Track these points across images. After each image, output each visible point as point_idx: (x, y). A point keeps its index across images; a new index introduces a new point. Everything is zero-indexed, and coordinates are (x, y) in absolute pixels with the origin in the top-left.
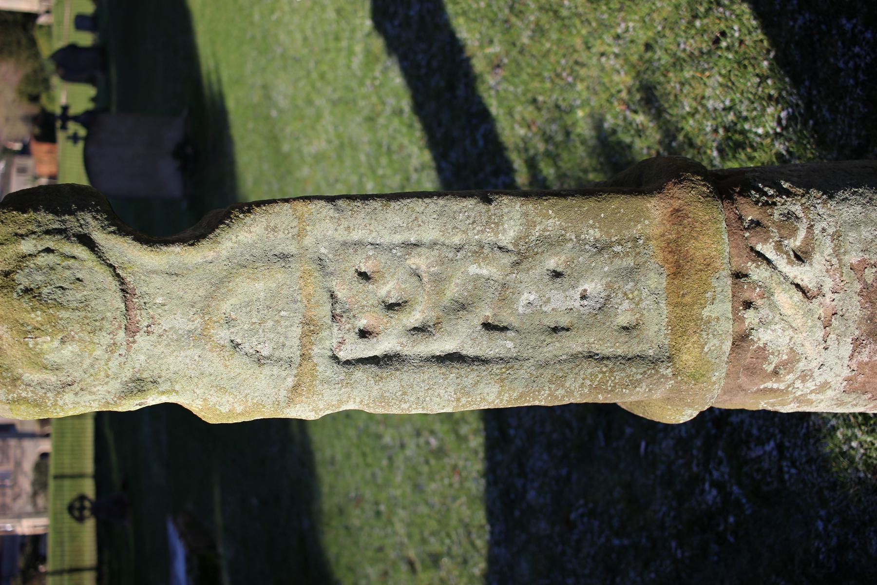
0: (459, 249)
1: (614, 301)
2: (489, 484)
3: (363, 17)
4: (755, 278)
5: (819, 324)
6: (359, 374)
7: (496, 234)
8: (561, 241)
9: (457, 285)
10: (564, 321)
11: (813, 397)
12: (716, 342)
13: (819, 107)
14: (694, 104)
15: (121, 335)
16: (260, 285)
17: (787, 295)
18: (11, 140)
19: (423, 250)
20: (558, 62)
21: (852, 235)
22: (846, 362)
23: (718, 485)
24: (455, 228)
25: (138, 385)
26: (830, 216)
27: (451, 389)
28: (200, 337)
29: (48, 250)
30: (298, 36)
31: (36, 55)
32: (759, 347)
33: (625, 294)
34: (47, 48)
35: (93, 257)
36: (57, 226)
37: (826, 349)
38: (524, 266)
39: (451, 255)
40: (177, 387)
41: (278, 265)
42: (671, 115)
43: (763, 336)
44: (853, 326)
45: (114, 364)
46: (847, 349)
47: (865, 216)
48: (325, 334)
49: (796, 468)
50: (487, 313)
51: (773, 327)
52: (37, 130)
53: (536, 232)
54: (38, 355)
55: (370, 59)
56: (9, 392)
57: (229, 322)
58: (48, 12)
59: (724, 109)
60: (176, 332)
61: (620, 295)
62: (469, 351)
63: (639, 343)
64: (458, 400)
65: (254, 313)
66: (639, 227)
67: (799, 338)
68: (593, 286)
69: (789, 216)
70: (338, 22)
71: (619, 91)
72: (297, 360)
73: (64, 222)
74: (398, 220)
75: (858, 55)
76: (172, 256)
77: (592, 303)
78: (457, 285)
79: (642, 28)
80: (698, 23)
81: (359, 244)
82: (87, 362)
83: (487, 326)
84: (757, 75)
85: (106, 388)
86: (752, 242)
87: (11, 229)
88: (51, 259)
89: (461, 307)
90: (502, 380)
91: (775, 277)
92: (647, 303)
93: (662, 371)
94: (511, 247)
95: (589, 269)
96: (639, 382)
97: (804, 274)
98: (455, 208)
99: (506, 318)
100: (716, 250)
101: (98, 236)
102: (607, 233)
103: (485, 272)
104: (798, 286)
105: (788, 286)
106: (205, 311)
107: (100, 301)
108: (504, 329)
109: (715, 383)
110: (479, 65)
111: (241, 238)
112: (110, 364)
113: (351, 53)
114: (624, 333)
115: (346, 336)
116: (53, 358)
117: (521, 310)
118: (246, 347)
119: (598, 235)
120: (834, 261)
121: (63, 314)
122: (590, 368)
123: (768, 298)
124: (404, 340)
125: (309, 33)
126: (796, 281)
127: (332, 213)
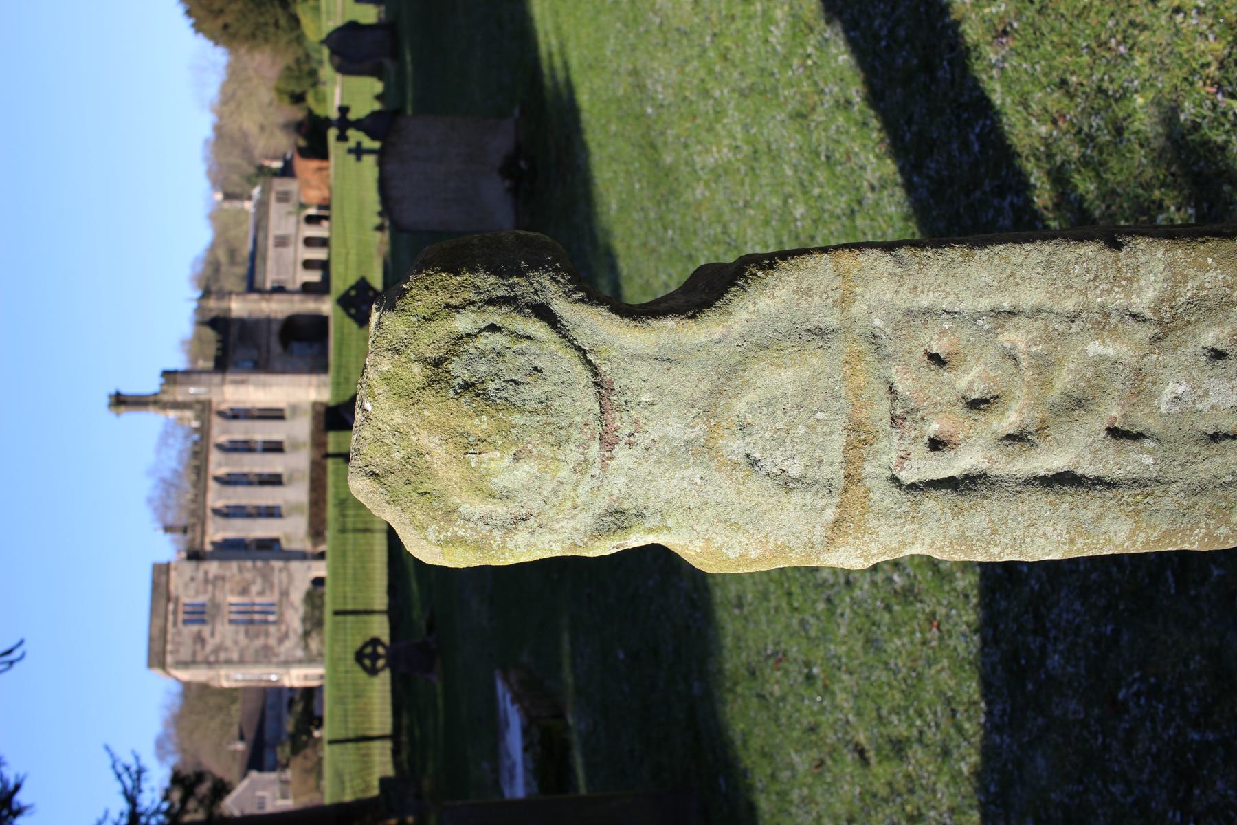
0: (1073, 318)
2: (984, 642)
6: (931, 503)
7: (1128, 295)
9: (1070, 371)
15: (595, 447)
16: (787, 375)
18: (267, 157)
19: (1020, 320)
24: (1068, 286)
27: (1062, 526)
28: (703, 450)
29: (493, 328)
31: (300, 39)
35: (555, 336)
38: (1170, 341)
39: (1062, 328)
41: (813, 345)
45: (584, 490)
52: (302, 143)
53: (1187, 291)
54: (483, 477)
57: (744, 428)
62: (1088, 469)
65: (779, 414)
72: (840, 483)
73: (511, 286)
74: (986, 277)
76: (664, 334)
81: (928, 313)
83: (1114, 432)
85: (572, 523)
87: (441, 298)
88: (496, 340)
89: (1077, 404)
90: (1137, 513)
94: (1148, 314)
98: (1069, 257)
99: (1141, 420)
101: (561, 307)
103: (1110, 352)
106: (710, 413)
107: (566, 400)
108: (1139, 437)
111: (760, 306)
112: (580, 490)
113: (768, 19)
116: (502, 481)
117: (1164, 408)
118: (768, 465)
121: (518, 419)
124: (994, 454)
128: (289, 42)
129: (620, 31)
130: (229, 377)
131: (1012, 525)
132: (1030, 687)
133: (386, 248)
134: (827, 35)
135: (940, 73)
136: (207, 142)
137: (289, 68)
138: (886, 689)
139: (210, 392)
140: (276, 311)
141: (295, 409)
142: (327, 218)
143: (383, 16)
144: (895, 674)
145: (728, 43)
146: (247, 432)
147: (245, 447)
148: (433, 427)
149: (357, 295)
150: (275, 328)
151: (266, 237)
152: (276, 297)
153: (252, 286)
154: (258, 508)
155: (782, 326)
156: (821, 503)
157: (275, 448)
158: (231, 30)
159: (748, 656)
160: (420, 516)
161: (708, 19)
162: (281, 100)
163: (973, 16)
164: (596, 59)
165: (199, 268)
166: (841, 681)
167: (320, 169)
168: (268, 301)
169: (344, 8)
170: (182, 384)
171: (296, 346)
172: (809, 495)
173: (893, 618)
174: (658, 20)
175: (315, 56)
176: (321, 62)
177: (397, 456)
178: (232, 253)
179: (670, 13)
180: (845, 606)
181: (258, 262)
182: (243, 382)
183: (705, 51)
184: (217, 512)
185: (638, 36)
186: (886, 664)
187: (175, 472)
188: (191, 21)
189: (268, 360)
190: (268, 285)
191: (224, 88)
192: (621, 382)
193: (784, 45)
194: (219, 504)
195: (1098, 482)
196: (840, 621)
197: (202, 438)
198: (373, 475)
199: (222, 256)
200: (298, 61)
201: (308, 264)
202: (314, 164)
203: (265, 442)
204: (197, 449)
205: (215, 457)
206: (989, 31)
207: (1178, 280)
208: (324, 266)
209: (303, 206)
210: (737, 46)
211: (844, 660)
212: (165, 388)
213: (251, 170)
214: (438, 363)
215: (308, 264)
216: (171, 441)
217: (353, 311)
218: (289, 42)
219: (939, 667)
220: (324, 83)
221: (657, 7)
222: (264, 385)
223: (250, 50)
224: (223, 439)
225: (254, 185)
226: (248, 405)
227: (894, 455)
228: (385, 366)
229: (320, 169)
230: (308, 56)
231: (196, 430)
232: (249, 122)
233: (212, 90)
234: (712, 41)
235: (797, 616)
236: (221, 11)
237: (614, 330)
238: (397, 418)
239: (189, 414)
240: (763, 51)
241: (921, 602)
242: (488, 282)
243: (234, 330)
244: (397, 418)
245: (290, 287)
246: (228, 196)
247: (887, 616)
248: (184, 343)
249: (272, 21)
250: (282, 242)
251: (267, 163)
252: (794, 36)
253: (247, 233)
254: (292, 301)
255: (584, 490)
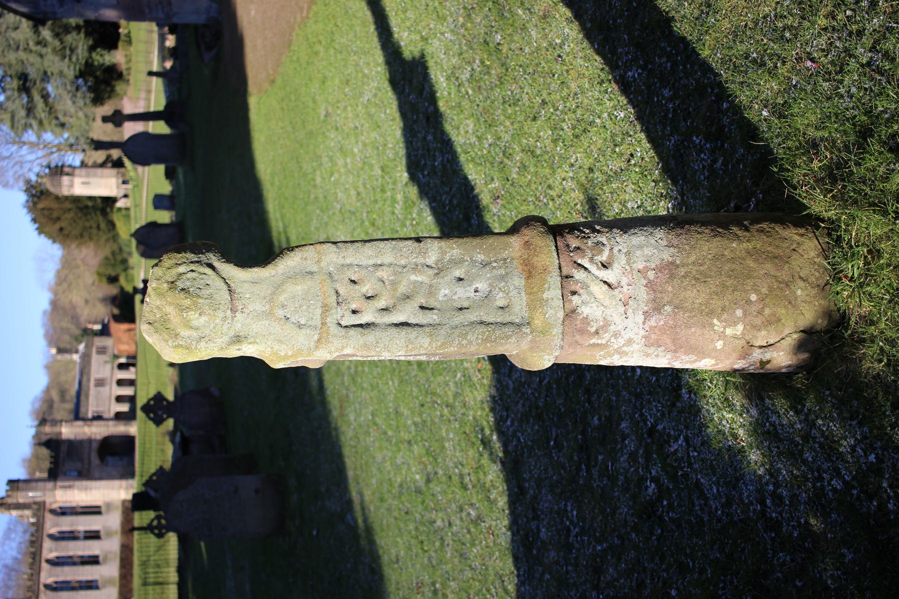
0: (404, 267)
1: (493, 293)
2: (513, 534)
3: (401, 171)
4: (577, 278)
5: (620, 303)
6: (352, 332)
7: (425, 258)
8: (462, 261)
9: (404, 286)
10: (466, 304)
11: (625, 349)
12: (552, 311)
13: (687, 197)
14: (620, 206)
15: (229, 312)
16: (299, 288)
17: (598, 287)
18: (90, 323)
19: (384, 268)
20: (537, 189)
21: (638, 253)
22: (641, 326)
23: (655, 480)
24: (401, 256)
25: (237, 339)
26: (624, 243)
27: (403, 341)
28: (270, 314)
29: (192, 271)
30: (353, 192)
31: (115, 237)
32: (584, 318)
33: (500, 289)
34: (125, 230)
35: (214, 273)
36: (196, 259)
37: (627, 318)
38: (442, 274)
39: (400, 270)
40: (258, 341)
41: (308, 277)
42: (608, 217)
43: (585, 311)
44: (643, 305)
45: (225, 327)
46: (640, 318)
47: (647, 242)
48: (333, 311)
49: (696, 451)
50: (423, 301)
51: (590, 305)
52: (116, 311)
53: (447, 257)
54: (188, 321)
55: (408, 205)
56: (174, 341)
57: (283, 306)
58: (126, 196)
59: (638, 207)
60: (256, 312)
61: (497, 289)
62: (412, 321)
63: (509, 316)
64: (407, 346)
65: (297, 302)
66: (506, 252)
67: (608, 312)
68: (482, 286)
69: (598, 243)
70: (383, 177)
71: (576, 205)
72: (319, 326)
73: (199, 258)
74: (370, 253)
75: (704, 160)
76: (254, 273)
77: (481, 294)
78: (404, 286)
79: (585, 157)
80: (617, 150)
81: (350, 266)
82: (212, 326)
83: (422, 308)
84: (654, 181)
85: (221, 340)
86: (575, 258)
87: (174, 261)
88: (193, 275)
89: (407, 297)
90: (431, 335)
91: (589, 277)
92: (514, 293)
93: (524, 330)
94: (433, 265)
95: (478, 275)
96: (511, 336)
97: (609, 275)
98: (401, 245)
99: (432, 303)
100: (549, 261)
101: (217, 264)
102: (488, 256)
103: (419, 279)
104: (605, 282)
105: (598, 282)
106: (271, 301)
107: (218, 295)
108: (432, 309)
109: (555, 336)
110: (485, 199)
111: (288, 263)
112: (224, 328)
113: (394, 201)
114: (501, 310)
115: (345, 313)
116: (195, 323)
117: (440, 299)
118: (293, 320)
119: (483, 258)
120: (627, 267)
121: (200, 301)
122: (482, 329)
123: (586, 289)
124: (376, 315)
125: (361, 189)
126: (604, 280)
127: (335, 249)
128: (107, 240)
129: (319, 215)
130: (59, 483)
131: (384, 340)
132: (535, 552)
133: (176, 378)
134: (422, 207)
135: (473, 221)
136: (45, 312)
137: (107, 258)
138: (471, 581)
139: (45, 495)
140: (95, 434)
141: (109, 506)
142: (134, 365)
143: (174, 218)
144: (475, 571)
145: (375, 216)
146: (72, 525)
147: (71, 536)
148: (170, 304)
149: (155, 404)
150: (95, 446)
151: (89, 380)
152: (95, 423)
153: (77, 415)
154: (80, 582)
155: (297, 271)
156: (313, 333)
157: (94, 536)
158: (65, 232)
159: (404, 592)
160: (166, 336)
161: (364, 203)
162: (100, 281)
163: (485, 189)
164: (306, 234)
165: (37, 405)
166: (450, 586)
167: (130, 330)
168: (89, 426)
169: (147, 214)
170: (23, 490)
171: (110, 459)
172: (308, 331)
173: (472, 537)
174: (339, 207)
175: (126, 249)
176: (130, 254)
177: (158, 316)
178: (63, 393)
179: (345, 202)
180: (448, 540)
181: (83, 398)
182: (70, 487)
183: (363, 222)
184: (47, 587)
185: (329, 217)
186: (470, 566)
187: (15, 559)
188: (36, 226)
189: (89, 470)
190: (90, 415)
191: (58, 273)
192: (238, 290)
193: (402, 214)
194: (50, 581)
195: (417, 325)
196: (447, 549)
197: (37, 531)
198: (150, 323)
199: (55, 395)
200: (113, 253)
201: (119, 399)
202: (125, 326)
203: (86, 532)
204: (34, 539)
205: (47, 544)
206: (491, 197)
207: (444, 253)
208: (132, 400)
209: (116, 357)
210: (380, 217)
211: (451, 573)
212: (10, 493)
213: (78, 332)
214: (172, 283)
215: (119, 399)
216: (13, 535)
217: (152, 415)
218: (107, 240)
219: (495, 558)
220: (132, 268)
221: (339, 199)
222: (86, 489)
223: (79, 246)
224: (54, 531)
225: (81, 342)
226: (74, 505)
227: (339, 316)
228: (154, 285)
229: (130, 330)
230: (121, 250)
231: (33, 524)
232: (77, 297)
233: (50, 276)
234: (367, 216)
235: (427, 554)
236: (58, 219)
237: (236, 272)
238: (158, 303)
239: (27, 512)
240: (392, 219)
241: (484, 522)
242: (191, 256)
243: (64, 448)
244: (158, 303)
245: (106, 416)
246: (60, 351)
247: (468, 536)
248: (24, 461)
249: (95, 225)
250: (100, 383)
251: (90, 326)
252: (406, 209)
253: (74, 377)
254: (108, 426)
255: (225, 327)
